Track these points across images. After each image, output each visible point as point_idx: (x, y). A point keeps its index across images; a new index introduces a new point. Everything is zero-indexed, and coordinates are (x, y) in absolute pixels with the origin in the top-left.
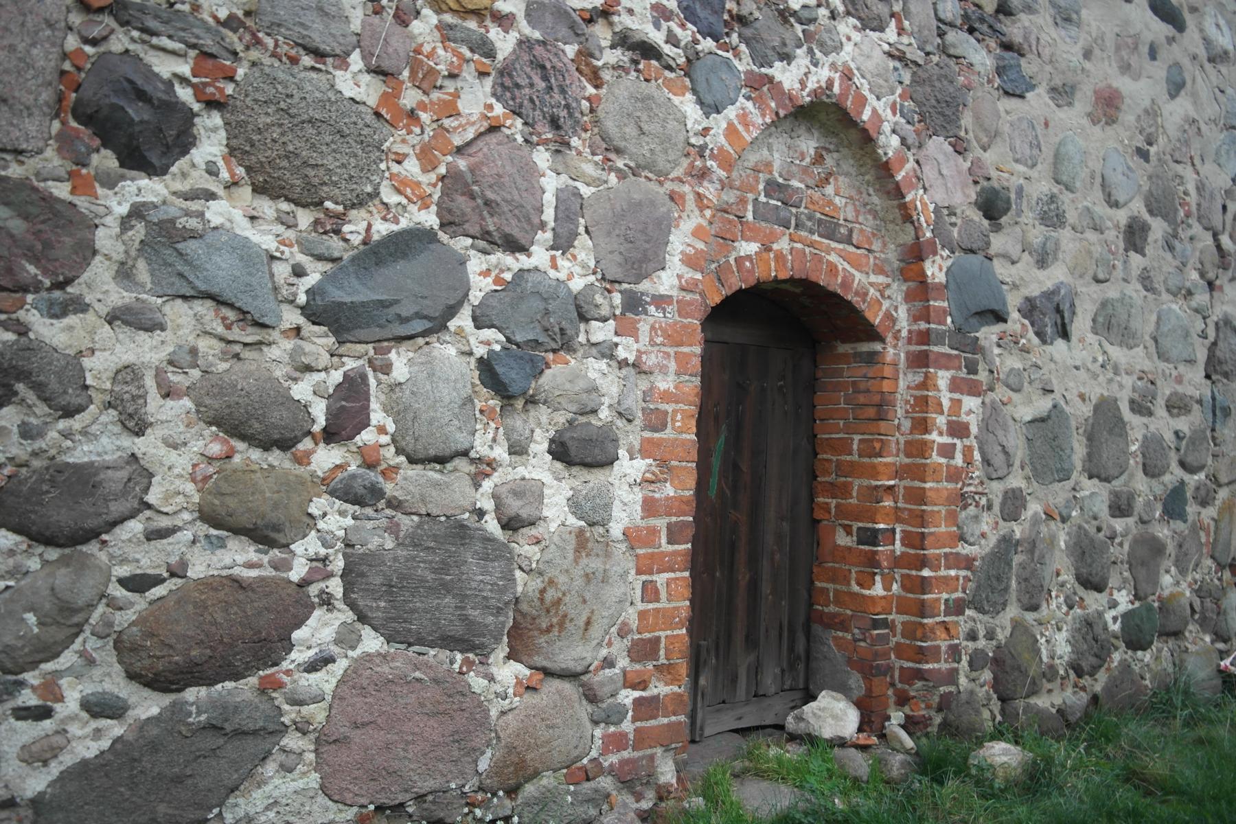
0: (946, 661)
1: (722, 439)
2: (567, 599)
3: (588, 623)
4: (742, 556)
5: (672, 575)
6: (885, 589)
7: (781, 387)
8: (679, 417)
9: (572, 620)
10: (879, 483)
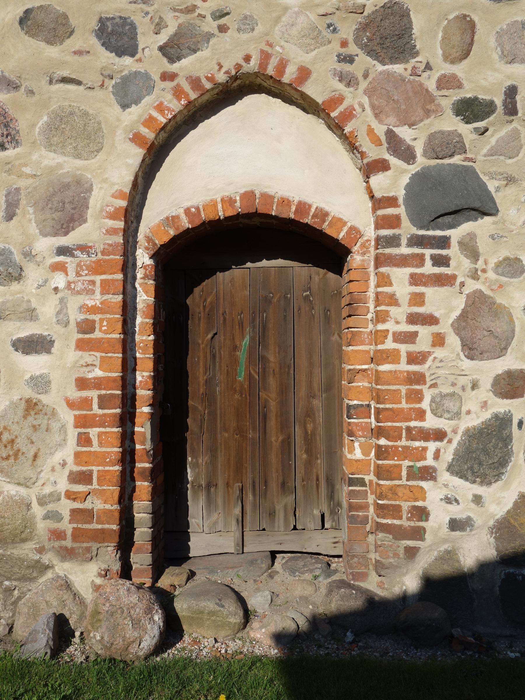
0: (408, 519)
1: (247, 339)
2: (18, 440)
3: (35, 456)
4: (273, 423)
5: (102, 430)
6: (363, 454)
7: (307, 296)
8: (105, 323)
9: (23, 453)
10: (352, 367)
